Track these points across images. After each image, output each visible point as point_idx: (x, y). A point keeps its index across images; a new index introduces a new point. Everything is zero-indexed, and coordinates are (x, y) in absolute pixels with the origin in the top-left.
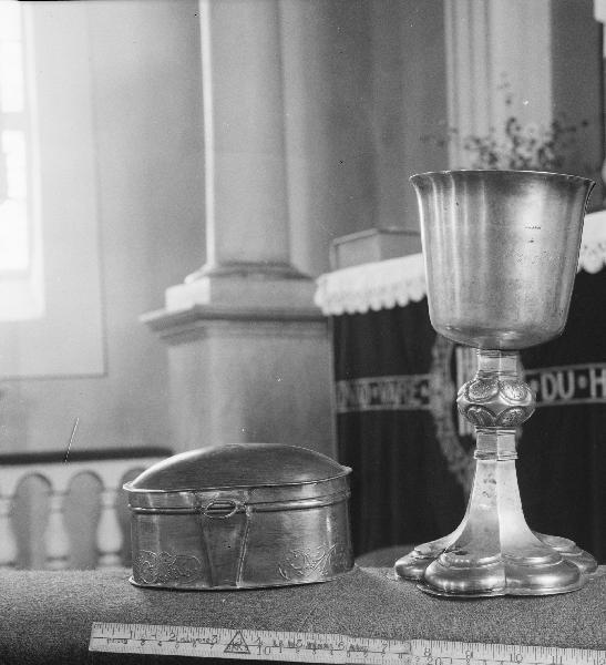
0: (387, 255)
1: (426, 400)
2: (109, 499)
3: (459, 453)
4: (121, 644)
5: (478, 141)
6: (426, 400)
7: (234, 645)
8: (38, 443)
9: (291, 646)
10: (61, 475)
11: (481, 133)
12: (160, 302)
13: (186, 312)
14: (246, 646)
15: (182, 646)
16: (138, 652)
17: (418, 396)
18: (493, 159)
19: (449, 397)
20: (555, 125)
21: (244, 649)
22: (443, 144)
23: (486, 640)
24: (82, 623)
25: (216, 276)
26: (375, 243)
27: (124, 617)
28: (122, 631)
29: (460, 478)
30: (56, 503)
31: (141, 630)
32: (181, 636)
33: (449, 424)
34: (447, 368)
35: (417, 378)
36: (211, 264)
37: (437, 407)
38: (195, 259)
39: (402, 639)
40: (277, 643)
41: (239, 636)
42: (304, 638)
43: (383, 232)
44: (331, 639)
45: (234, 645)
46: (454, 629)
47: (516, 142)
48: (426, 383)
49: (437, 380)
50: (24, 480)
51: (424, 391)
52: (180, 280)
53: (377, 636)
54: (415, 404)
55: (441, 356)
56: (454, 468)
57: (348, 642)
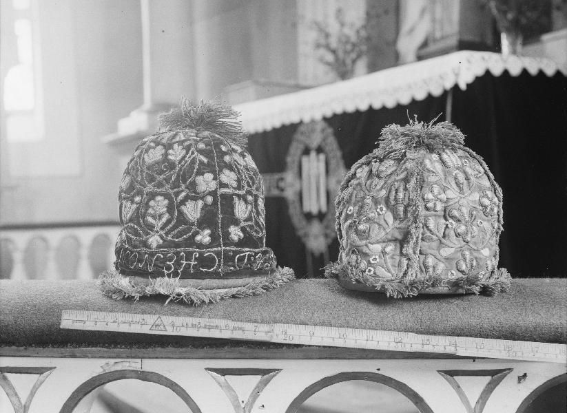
0: (260, 96)
1: (282, 190)
2: (84, 252)
3: (304, 223)
4: (82, 324)
5: (316, 23)
6: (282, 190)
7: (156, 326)
8: (40, 218)
9: (194, 326)
10: (55, 236)
11: (320, 19)
12: (114, 129)
13: (132, 136)
14: (164, 326)
15: (122, 325)
16: (93, 329)
17: (278, 187)
18: (327, 36)
19: (297, 186)
20: (368, 14)
21: (162, 327)
22: (294, 25)
23: (323, 324)
24: (56, 310)
25: (152, 112)
26: (251, 90)
27: (84, 307)
28: (82, 315)
29: (304, 240)
30: (51, 254)
31: (99, 315)
32: (120, 320)
33: (297, 205)
34: (296, 169)
35: (276, 176)
36: (147, 104)
37: (290, 194)
38: (137, 102)
39: (267, 322)
40: (185, 324)
41: (159, 320)
42: (203, 321)
43: (257, 83)
44: (217, 322)
45: (156, 326)
46: (302, 317)
47: (342, 25)
48: (282, 179)
49: (289, 177)
50: (31, 243)
51: (282, 184)
52: (127, 114)
53: (249, 321)
54: (275, 192)
55: (294, 162)
56: (300, 233)
57: (232, 324)
